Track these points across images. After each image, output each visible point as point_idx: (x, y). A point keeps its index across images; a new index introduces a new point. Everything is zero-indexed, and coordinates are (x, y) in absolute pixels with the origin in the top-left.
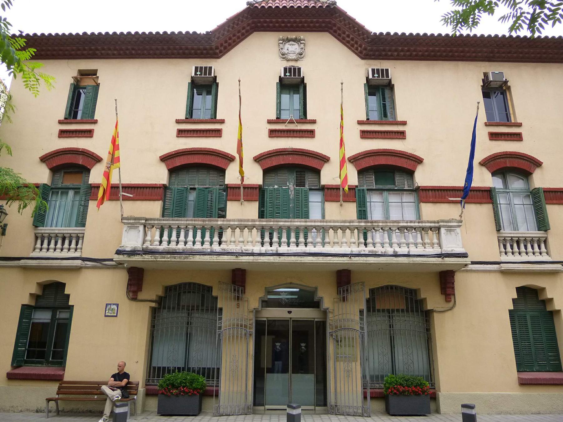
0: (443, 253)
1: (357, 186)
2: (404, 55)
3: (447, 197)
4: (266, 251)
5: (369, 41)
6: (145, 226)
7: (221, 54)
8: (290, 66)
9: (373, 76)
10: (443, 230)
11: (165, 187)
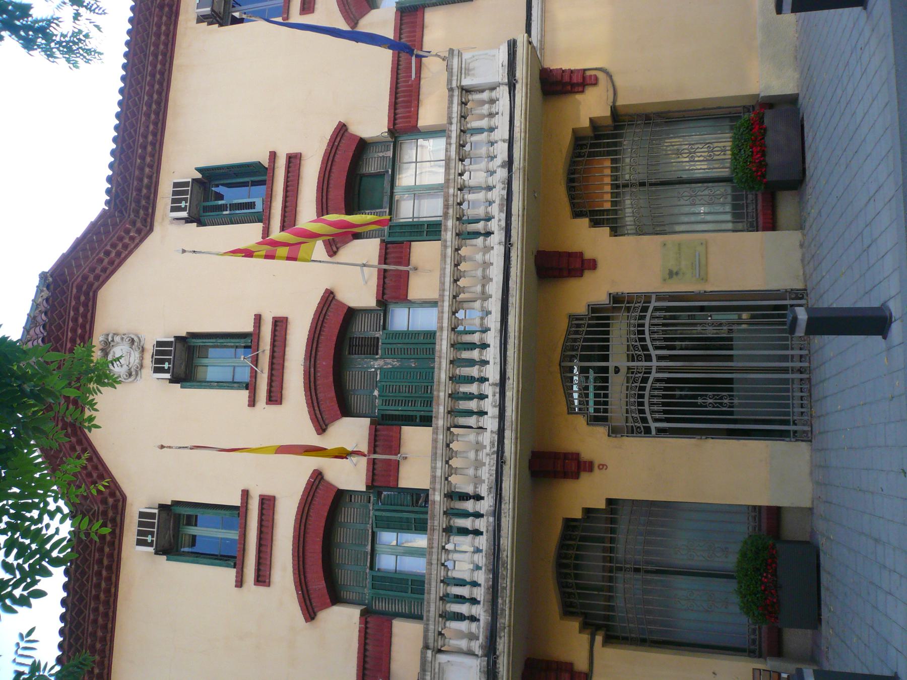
0: (507, 81)
1: (382, 241)
2: (152, 156)
3: (410, 83)
4: (495, 406)
5: (119, 215)
6: (440, 651)
7: (118, 493)
8: (152, 361)
9: (184, 209)
10: (467, 82)
11: (366, 614)
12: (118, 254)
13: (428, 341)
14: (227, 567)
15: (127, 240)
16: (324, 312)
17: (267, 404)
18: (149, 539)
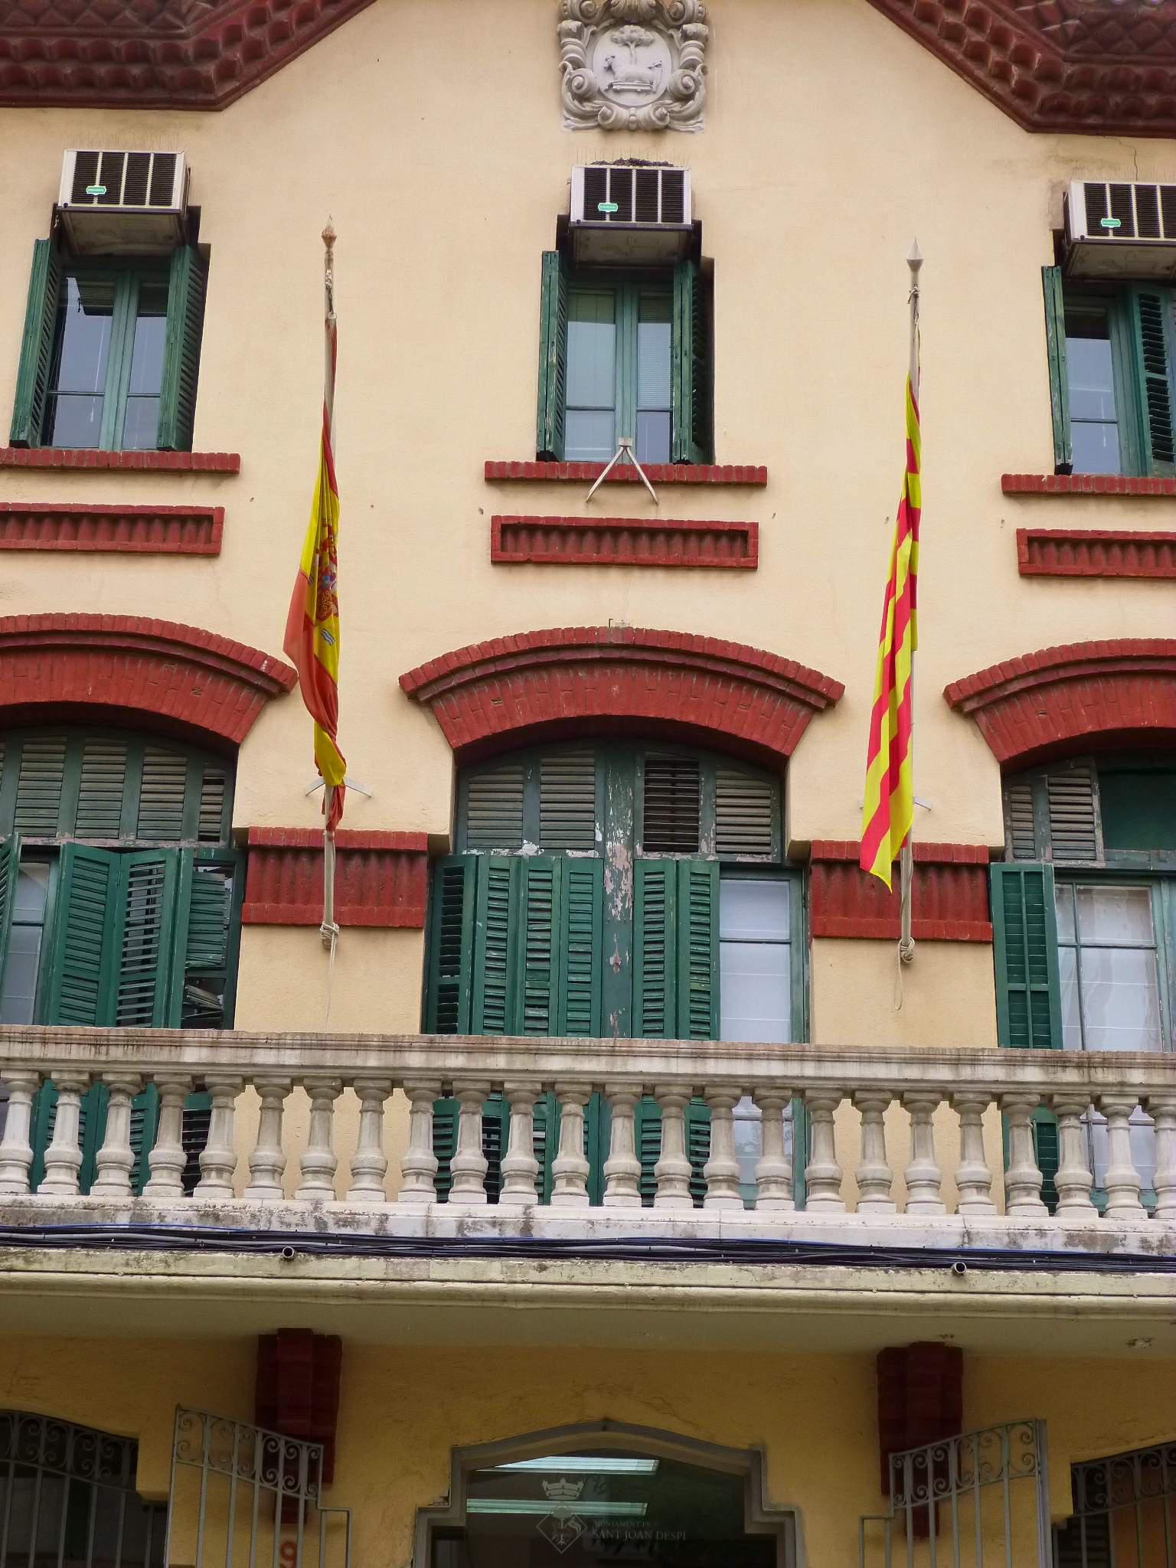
1: (997, 854)
4: (461, 1226)
5: (1071, 31)
8: (621, 162)
9: (1094, 226)
12: (954, 34)
13: (685, 1015)
14: (15, 421)
15: (994, 56)
16: (771, 682)
17: (495, 519)
18: (97, 189)
